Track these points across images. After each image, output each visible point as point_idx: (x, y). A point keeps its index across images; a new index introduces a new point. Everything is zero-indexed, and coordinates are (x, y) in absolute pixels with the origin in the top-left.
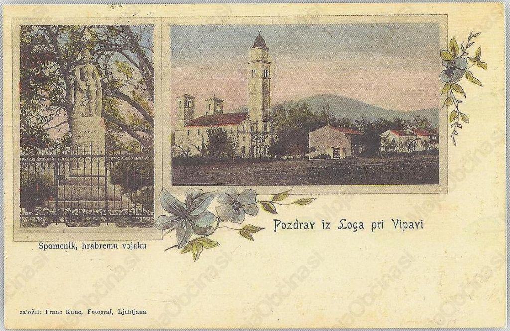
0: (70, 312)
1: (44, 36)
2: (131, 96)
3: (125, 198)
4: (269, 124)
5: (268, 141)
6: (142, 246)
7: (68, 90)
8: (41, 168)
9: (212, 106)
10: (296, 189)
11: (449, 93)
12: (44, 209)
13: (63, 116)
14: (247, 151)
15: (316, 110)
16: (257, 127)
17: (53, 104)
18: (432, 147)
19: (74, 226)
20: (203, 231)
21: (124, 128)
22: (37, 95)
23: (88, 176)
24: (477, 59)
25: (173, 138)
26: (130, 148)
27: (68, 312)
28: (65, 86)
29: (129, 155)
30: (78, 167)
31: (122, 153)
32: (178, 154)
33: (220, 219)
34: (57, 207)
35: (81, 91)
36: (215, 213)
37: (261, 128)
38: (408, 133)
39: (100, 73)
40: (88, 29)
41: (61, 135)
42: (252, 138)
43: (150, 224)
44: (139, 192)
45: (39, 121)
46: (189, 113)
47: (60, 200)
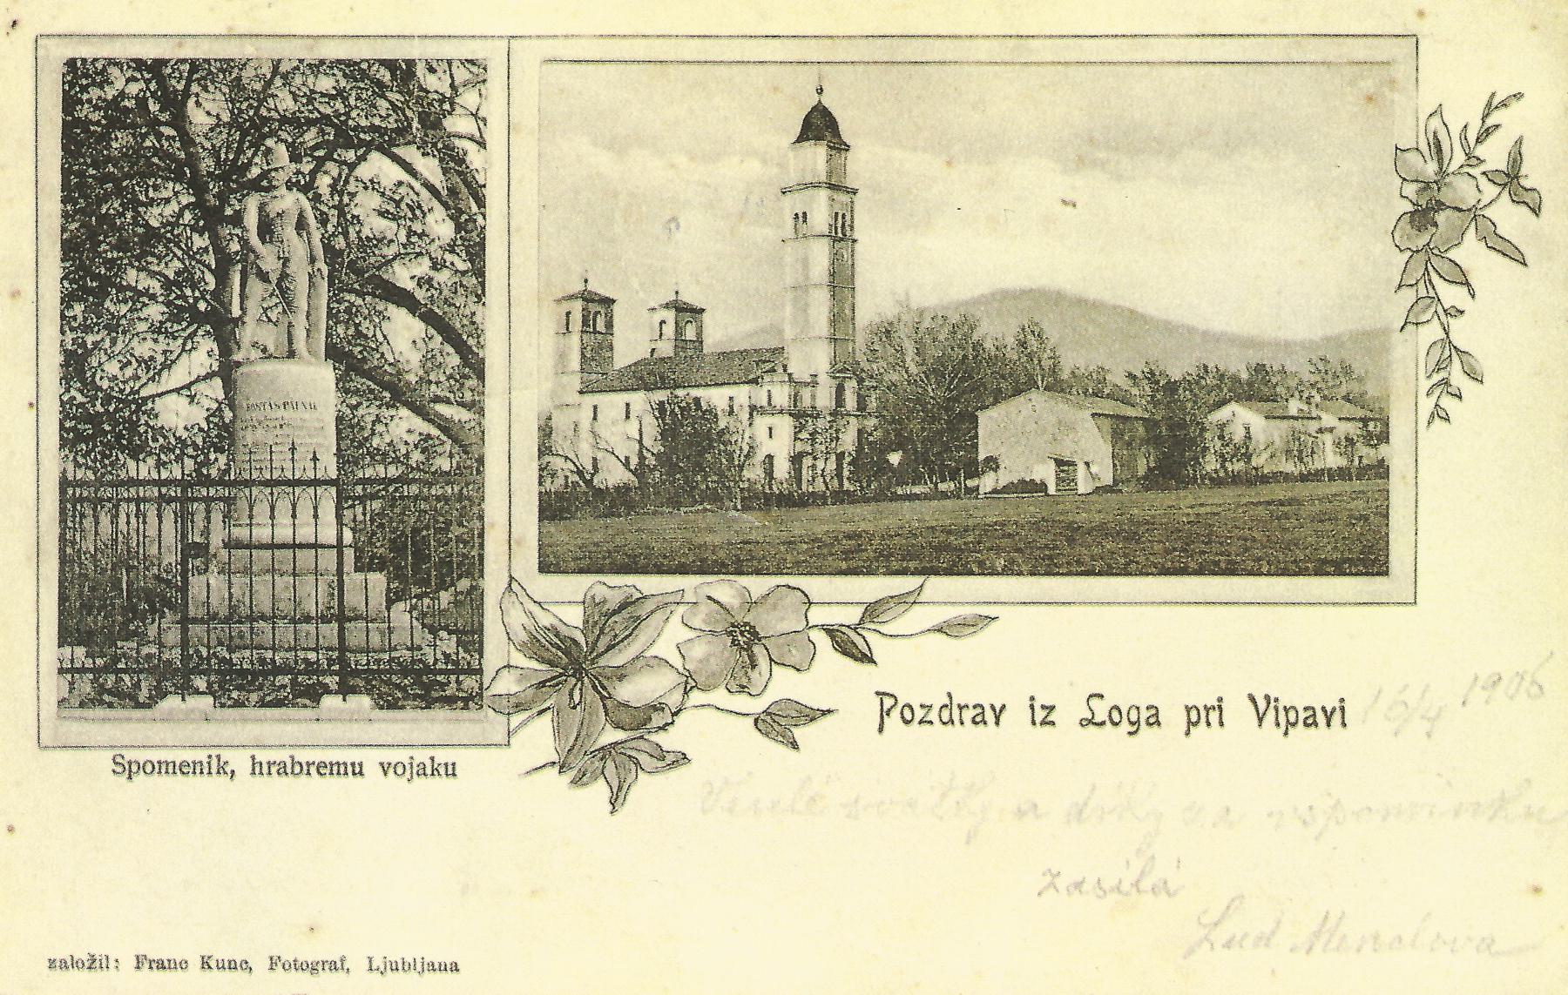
0: (213, 964)
1: (145, 99)
2: (421, 295)
3: (401, 615)
4: (851, 386)
5: (848, 441)
6: (442, 770)
7: (222, 275)
8: (133, 520)
9: (669, 330)
10: (938, 586)
11: (1421, 285)
12: (145, 650)
13: (203, 356)
14: (782, 469)
15: (996, 332)
16: (813, 397)
17: (175, 318)
18: (1368, 454)
19: (238, 704)
20: (641, 719)
21: (398, 393)
22: (121, 289)
23: (262, 546)
24: (1511, 179)
25: (546, 431)
26: (416, 456)
27: (205, 964)
28: (211, 259)
29: (414, 481)
30: (251, 517)
31: (393, 471)
32: (561, 481)
33: (689, 683)
34: (185, 644)
35: (264, 277)
36: (676, 661)
37: (824, 398)
38: (1293, 411)
39: (323, 220)
40: (285, 76)
41: (198, 415)
42: (799, 429)
43: (470, 700)
44: (445, 597)
45: (129, 372)
46: (596, 353)
47: (195, 621)
